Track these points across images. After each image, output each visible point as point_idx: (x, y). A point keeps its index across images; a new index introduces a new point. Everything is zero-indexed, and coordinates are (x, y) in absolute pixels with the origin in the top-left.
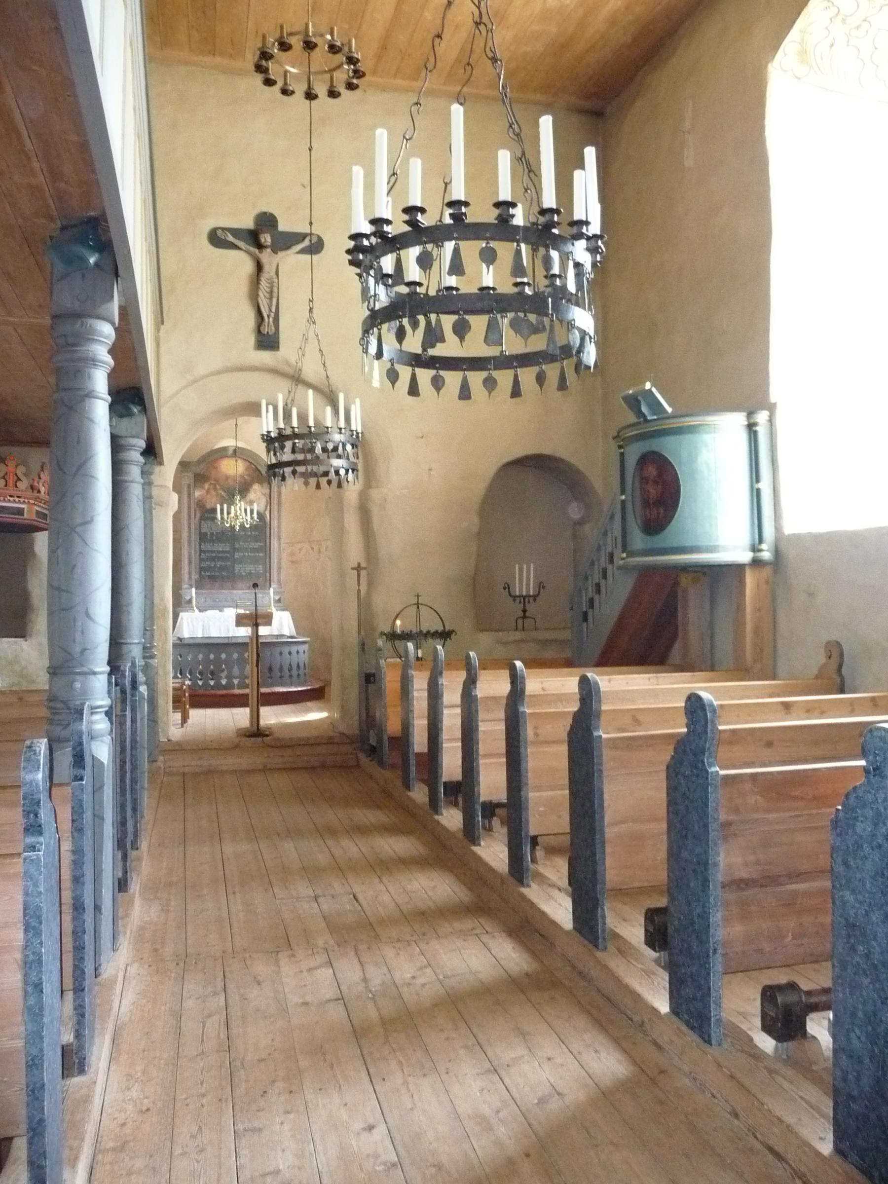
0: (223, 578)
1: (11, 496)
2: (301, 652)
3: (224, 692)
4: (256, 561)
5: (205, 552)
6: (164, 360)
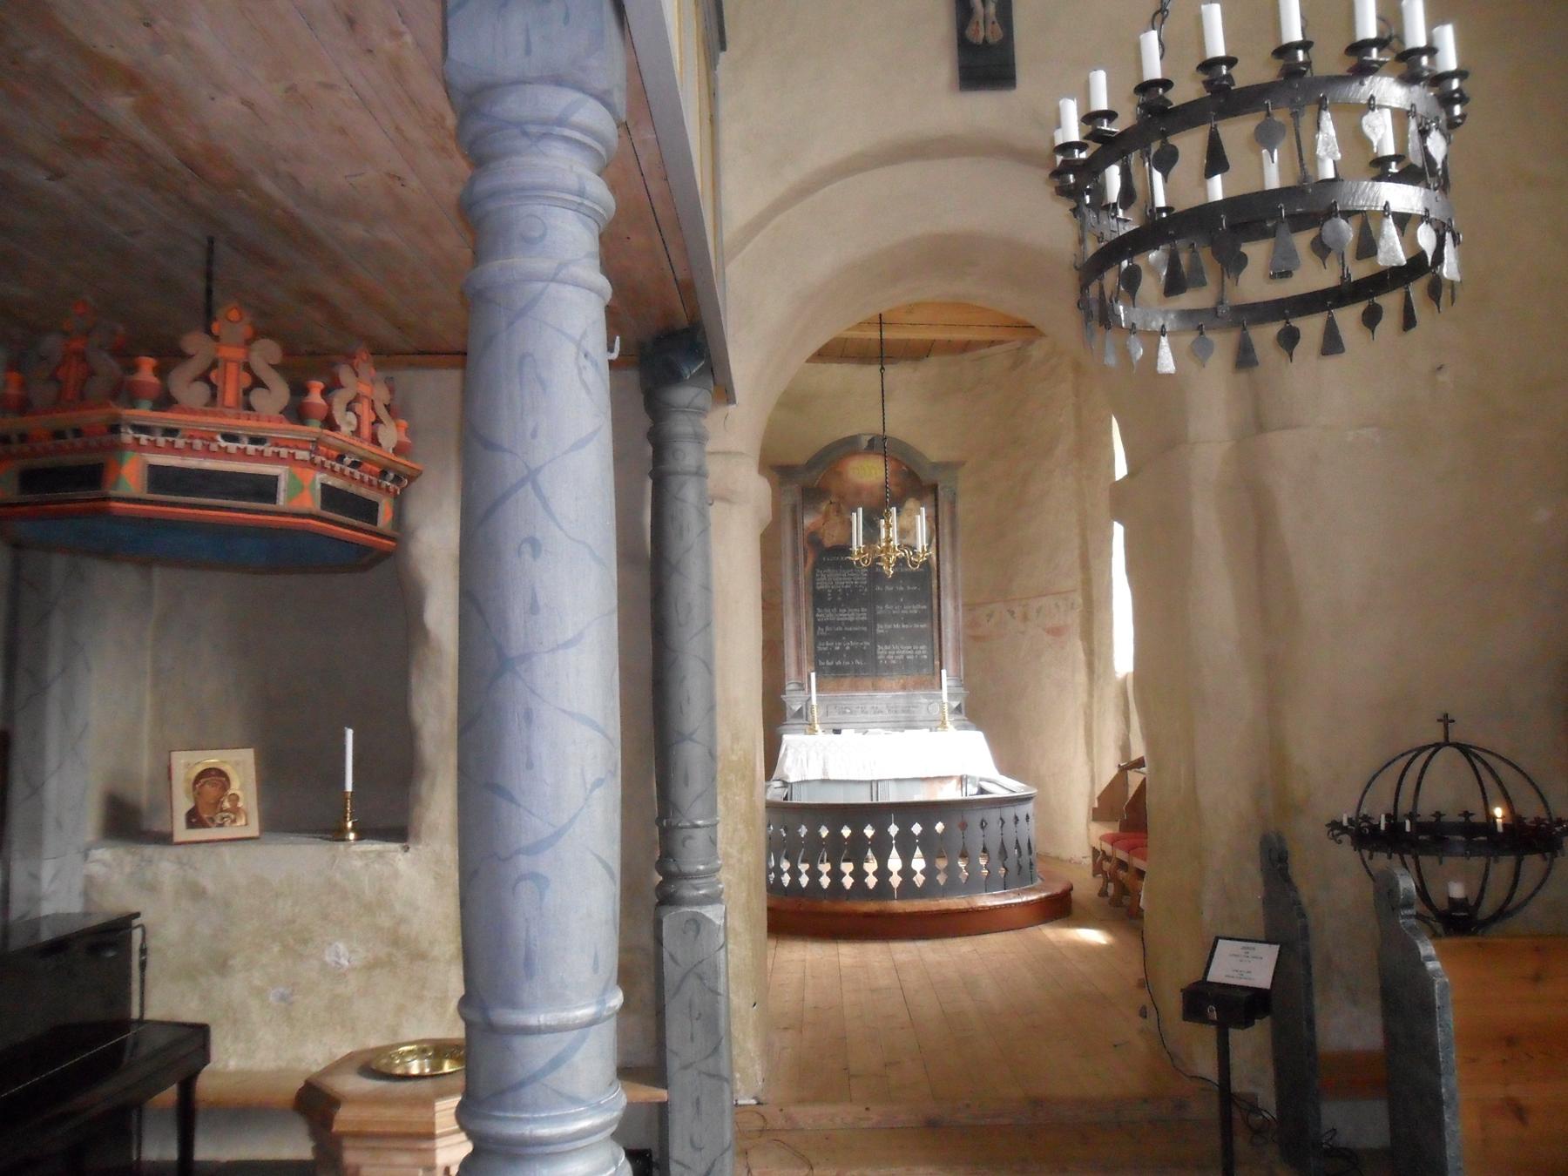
0: (857, 672)
1: (255, 440)
2: (1022, 818)
3: (872, 906)
4: (915, 638)
5: (823, 625)
6: (730, 134)
